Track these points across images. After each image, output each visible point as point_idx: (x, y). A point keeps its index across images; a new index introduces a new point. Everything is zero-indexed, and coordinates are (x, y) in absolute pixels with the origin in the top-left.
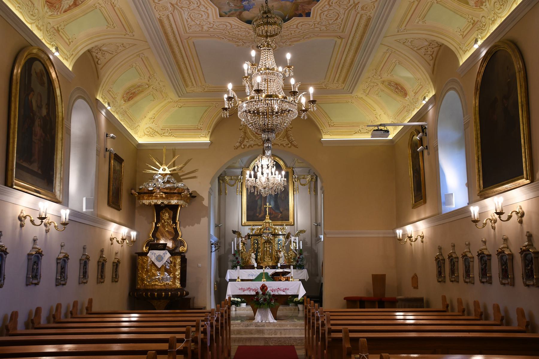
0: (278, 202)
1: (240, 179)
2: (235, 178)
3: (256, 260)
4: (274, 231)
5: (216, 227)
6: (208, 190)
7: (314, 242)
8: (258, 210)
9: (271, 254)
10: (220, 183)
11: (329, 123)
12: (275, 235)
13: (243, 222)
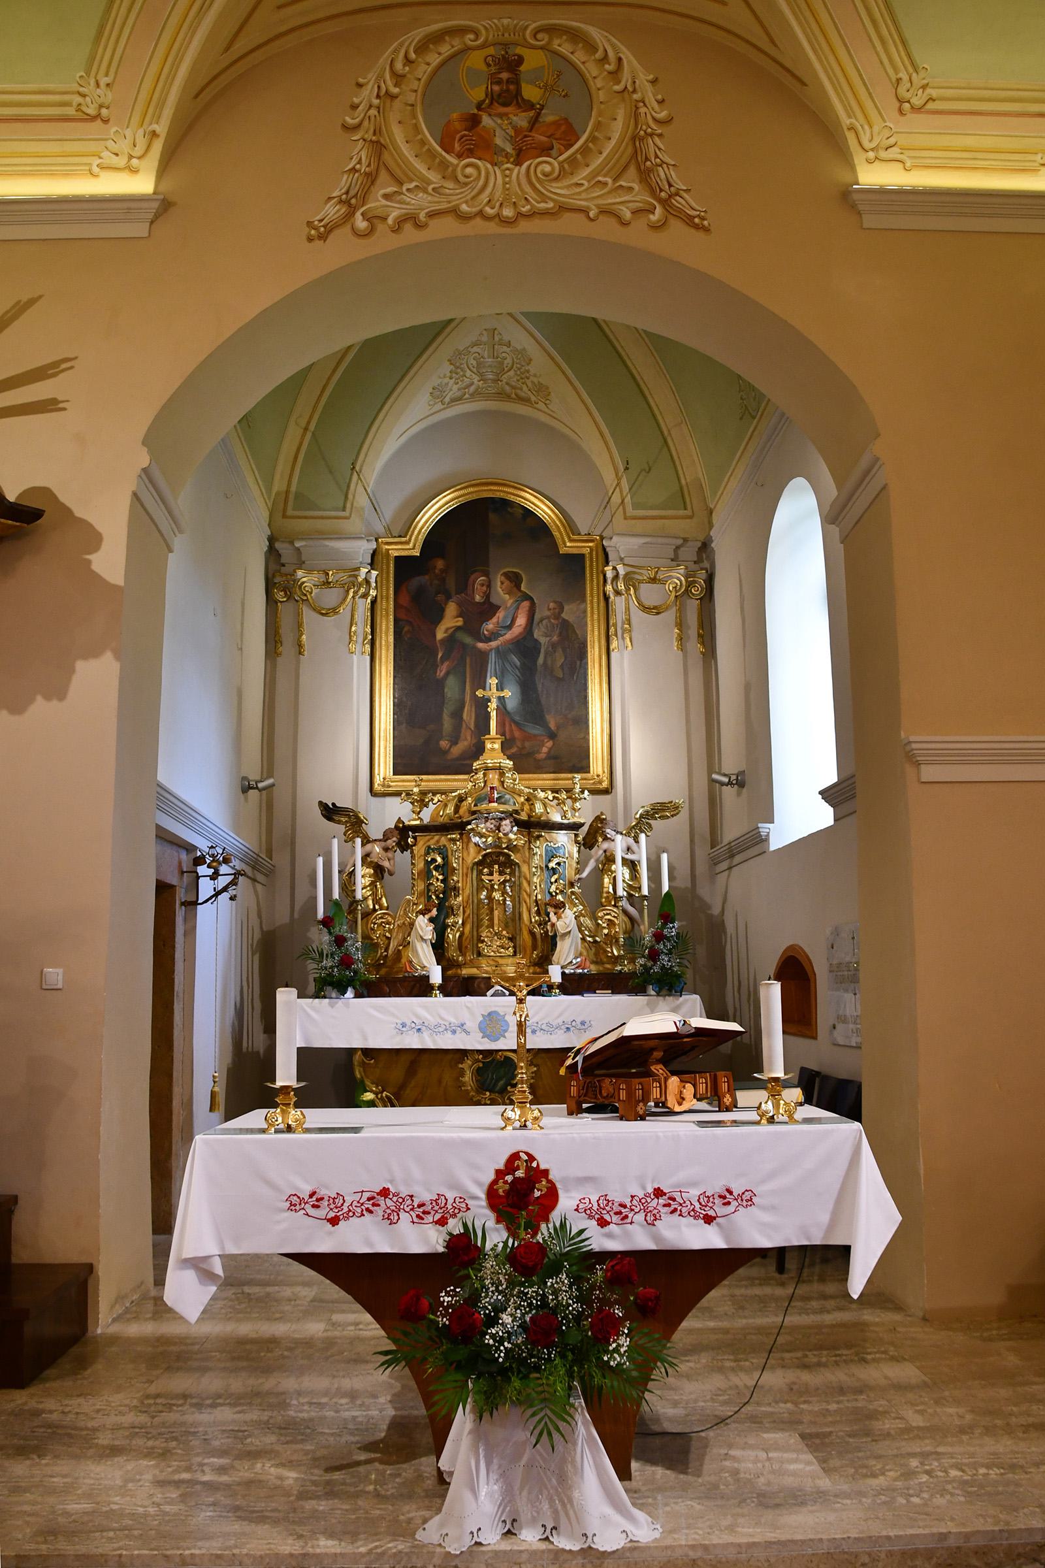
0: (540, 687)
1: (367, 582)
2: (344, 577)
3: (439, 947)
4: (526, 807)
6: (130, 484)
7: (702, 867)
8: (447, 723)
9: (513, 921)
10: (276, 602)
11: (902, 91)
12: (533, 826)
13: (378, 780)
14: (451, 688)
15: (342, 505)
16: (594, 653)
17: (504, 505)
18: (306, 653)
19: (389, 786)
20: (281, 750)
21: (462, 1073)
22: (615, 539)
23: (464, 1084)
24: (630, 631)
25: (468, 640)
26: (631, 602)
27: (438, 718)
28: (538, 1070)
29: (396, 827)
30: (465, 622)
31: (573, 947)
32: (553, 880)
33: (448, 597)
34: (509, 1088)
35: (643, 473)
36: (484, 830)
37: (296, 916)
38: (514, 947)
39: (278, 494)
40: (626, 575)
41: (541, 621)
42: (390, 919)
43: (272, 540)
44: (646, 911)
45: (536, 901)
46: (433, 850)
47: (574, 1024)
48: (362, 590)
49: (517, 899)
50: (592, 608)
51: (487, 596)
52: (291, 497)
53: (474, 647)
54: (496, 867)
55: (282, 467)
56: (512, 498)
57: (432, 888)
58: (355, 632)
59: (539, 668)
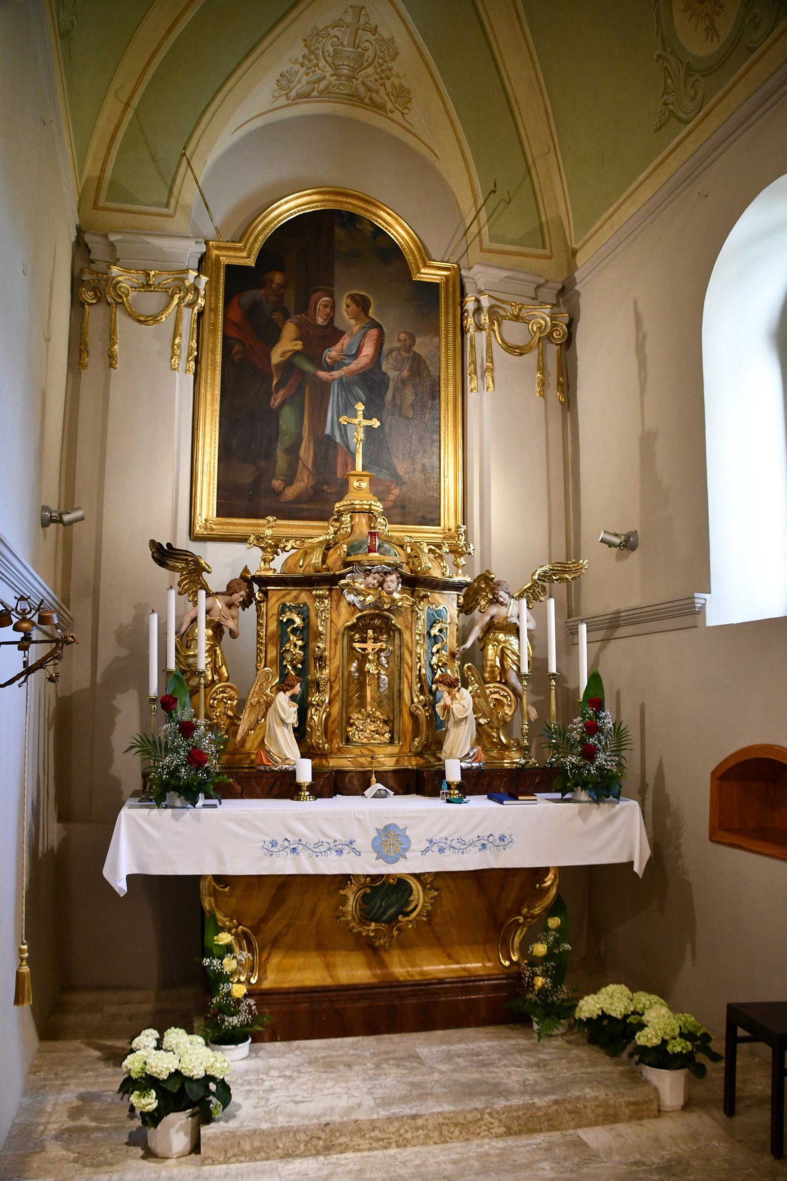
1: (197, 290)
2: (167, 279)
3: (301, 733)
5: (45, 523)
8: (281, 461)
10: (82, 304)
13: (200, 521)
14: (287, 420)
15: (165, 200)
16: (448, 393)
17: (350, 219)
18: (117, 366)
19: (212, 530)
20: (84, 482)
21: (344, 900)
22: (476, 268)
23: (344, 914)
24: (492, 370)
25: (308, 367)
27: (270, 456)
28: (440, 895)
29: (243, 577)
30: (304, 345)
31: (470, 736)
32: (434, 650)
33: (287, 317)
34: (400, 917)
35: (503, 204)
36: (362, 586)
37: (99, 680)
38: (392, 732)
39: (88, 180)
40: (492, 307)
41: (390, 352)
42: (233, 693)
43: (80, 231)
44: (553, 692)
45: (419, 676)
46: (290, 609)
47: (491, 839)
48: (190, 297)
49: (397, 674)
50: (447, 342)
51: (331, 320)
52: (105, 186)
53: (315, 376)
54: (370, 632)
55: (96, 147)
56: (361, 213)
58: (179, 346)
59: (386, 404)
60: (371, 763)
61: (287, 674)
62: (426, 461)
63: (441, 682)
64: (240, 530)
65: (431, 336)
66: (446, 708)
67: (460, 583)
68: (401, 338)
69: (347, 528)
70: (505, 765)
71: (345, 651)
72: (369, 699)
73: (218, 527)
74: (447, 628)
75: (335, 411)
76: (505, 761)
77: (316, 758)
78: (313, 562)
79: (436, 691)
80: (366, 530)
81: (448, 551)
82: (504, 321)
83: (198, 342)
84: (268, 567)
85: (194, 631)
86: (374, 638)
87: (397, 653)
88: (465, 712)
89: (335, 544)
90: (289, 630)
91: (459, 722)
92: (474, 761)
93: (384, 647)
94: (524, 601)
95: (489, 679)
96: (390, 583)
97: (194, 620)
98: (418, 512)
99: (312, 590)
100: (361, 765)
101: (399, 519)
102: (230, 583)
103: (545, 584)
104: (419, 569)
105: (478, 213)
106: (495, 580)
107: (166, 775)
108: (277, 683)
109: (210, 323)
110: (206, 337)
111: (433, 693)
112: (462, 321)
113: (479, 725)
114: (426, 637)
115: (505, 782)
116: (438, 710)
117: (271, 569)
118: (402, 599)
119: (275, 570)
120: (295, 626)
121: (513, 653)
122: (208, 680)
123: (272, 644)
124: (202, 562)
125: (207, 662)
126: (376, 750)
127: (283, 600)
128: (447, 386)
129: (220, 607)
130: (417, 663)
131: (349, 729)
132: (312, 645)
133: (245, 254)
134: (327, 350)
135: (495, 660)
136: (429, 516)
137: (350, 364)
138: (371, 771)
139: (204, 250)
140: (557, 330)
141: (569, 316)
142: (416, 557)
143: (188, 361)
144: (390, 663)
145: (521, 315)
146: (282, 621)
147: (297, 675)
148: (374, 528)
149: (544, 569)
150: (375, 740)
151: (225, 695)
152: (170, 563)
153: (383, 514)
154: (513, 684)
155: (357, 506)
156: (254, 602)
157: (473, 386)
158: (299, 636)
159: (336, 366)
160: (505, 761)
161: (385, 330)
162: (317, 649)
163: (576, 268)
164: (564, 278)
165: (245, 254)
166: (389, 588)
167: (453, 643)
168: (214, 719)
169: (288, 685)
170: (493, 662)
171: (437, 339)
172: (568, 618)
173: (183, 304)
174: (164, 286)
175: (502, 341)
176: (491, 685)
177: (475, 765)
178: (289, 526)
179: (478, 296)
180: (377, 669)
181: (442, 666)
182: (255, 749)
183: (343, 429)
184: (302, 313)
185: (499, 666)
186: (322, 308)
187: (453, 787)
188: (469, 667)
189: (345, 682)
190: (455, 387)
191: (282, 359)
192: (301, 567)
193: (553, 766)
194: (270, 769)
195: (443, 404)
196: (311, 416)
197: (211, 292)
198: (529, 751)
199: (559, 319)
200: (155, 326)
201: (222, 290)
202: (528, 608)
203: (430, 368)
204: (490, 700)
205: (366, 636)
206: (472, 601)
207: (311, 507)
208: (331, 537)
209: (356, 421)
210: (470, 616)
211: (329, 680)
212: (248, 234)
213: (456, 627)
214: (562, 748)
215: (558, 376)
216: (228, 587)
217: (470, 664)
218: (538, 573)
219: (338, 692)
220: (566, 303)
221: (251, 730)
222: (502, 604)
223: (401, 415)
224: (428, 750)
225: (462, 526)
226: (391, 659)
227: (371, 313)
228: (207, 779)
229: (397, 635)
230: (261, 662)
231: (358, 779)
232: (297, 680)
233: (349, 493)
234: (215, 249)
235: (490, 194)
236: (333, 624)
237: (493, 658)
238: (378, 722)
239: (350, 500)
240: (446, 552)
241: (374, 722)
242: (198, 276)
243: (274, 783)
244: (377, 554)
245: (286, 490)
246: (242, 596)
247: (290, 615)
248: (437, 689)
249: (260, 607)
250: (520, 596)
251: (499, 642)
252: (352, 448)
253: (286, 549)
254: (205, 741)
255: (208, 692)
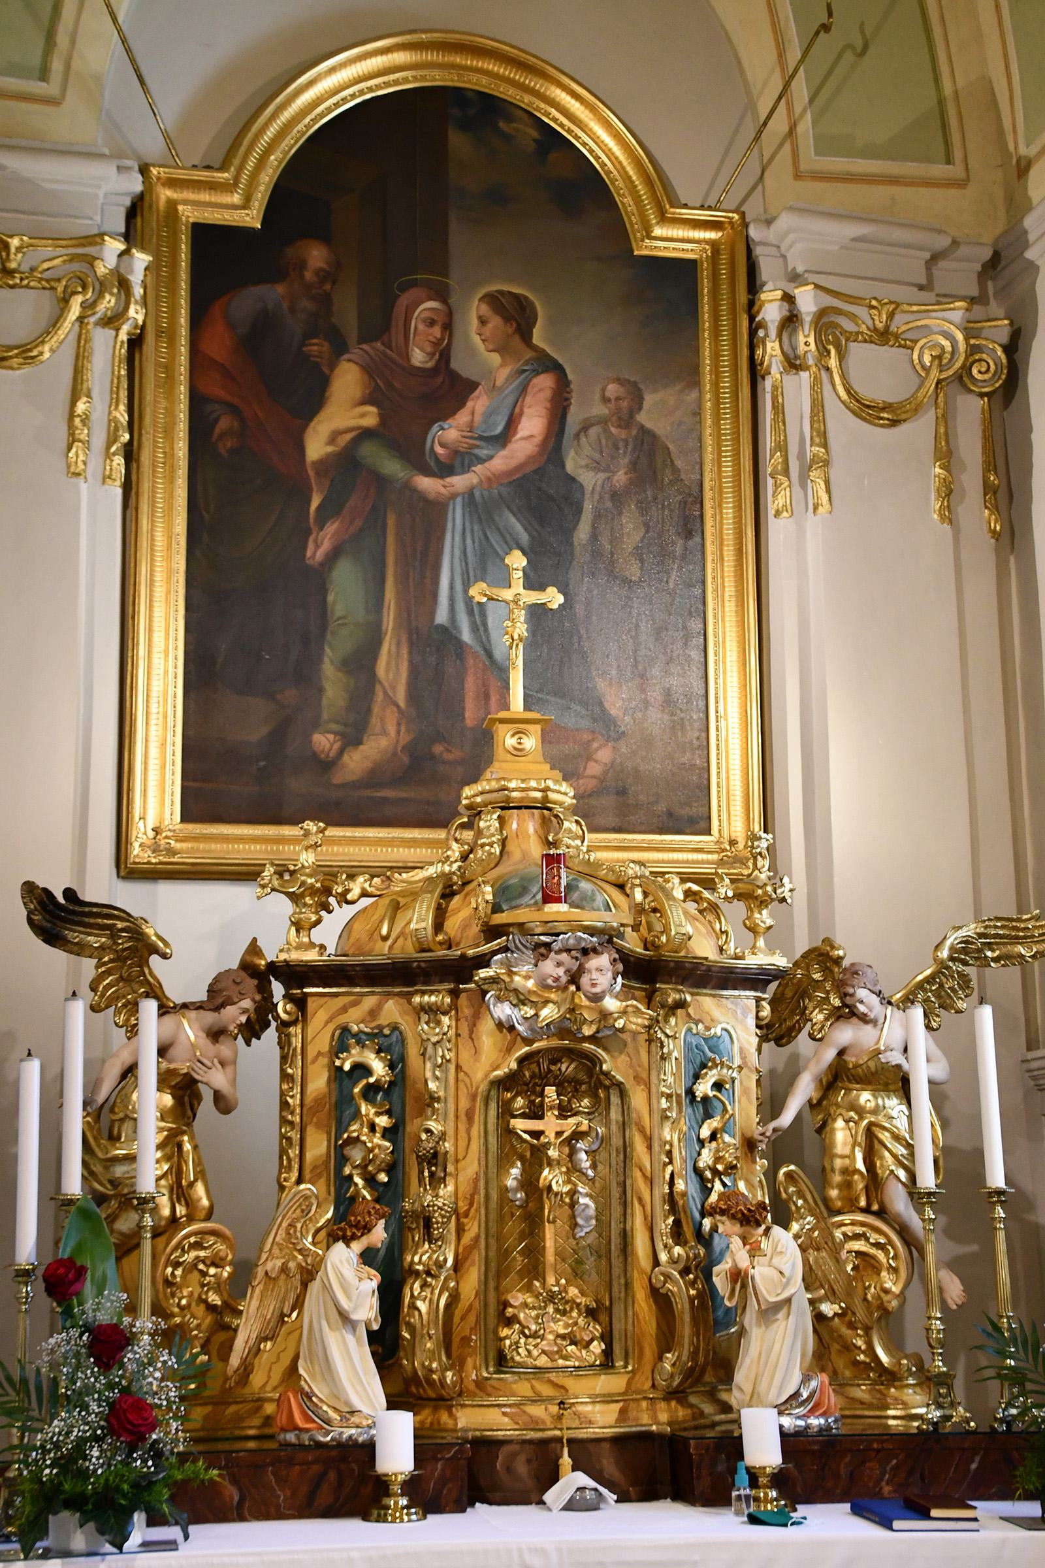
1: (124, 285)
13: (141, 833)
15: (36, 60)
19: (171, 852)
22: (785, 221)
24: (826, 463)
25: (392, 467)
26: (827, 387)
29: (247, 967)
30: (381, 416)
32: (705, 1132)
33: (340, 348)
35: (849, 56)
36: (530, 984)
40: (822, 313)
41: (585, 429)
42: (221, 1247)
44: (1001, 1236)
45: (671, 1198)
48: (109, 302)
49: (616, 1193)
50: (717, 401)
51: (444, 355)
53: (408, 487)
54: (551, 1091)
57: (357, 1155)
58: (86, 419)
59: (577, 550)
60: (560, 1417)
61: (353, 1199)
62: (674, 682)
63: (723, 1212)
64: (239, 851)
65: (678, 387)
66: (738, 1277)
67: (762, 970)
68: (607, 394)
69: (491, 845)
70: (891, 1422)
71: (493, 1140)
72: (550, 1256)
73: (184, 845)
74: (733, 1080)
75: (458, 570)
76: (891, 1412)
77: (422, 1407)
78: (413, 926)
79: (711, 1235)
80: (536, 850)
81: (730, 894)
82: (852, 345)
83: (130, 410)
84: (306, 940)
85: (128, 1097)
86: (561, 1107)
87: (616, 1141)
88: (785, 1286)
89: (465, 884)
90: (356, 1090)
91: (770, 1312)
92: (812, 1411)
93: (584, 1127)
94: (917, 1012)
95: (839, 1204)
96: (595, 975)
97: (130, 1071)
98: (657, 802)
99: (412, 994)
100: (535, 1424)
101: (612, 820)
102: (216, 980)
103: (967, 970)
104: (664, 939)
105: (787, 85)
106: (846, 963)
107: (52, 1466)
108: (329, 1221)
109: (158, 364)
110: (149, 397)
111: (705, 1240)
112: (752, 348)
113: (819, 1318)
114: (685, 1101)
115: (894, 1469)
116: (719, 1281)
117: (312, 945)
118: (624, 1013)
119: (323, 947)
120: (372, 1080)
121: (897, 1138)
122: (161, 1218)
123: (318, 1126)
124: (150, 931)
125: (159, 1173)
126: (569, 1383)
127: (342, 1019)
128: (720, 506)
129: (192, 1038)
130: (665, 1165)
131: (505, 1332)
132: (412, 1126)
133: (236, 198)
134: (435, 427)
135: (852, 1157)
136: (683, 812)
137: (491, 457)
138: (559, 1440)
139: (138, 187)
140: (980, 360)
141: (1011, 324)
142: (655, 910)
143: (108, 455)
144: (600, 1167)
145: (893, 328)
146: (340, 1068)
147: (377, 1200)
148: (555, 844)
149: (962, 933)
150: (566, 1358)
151: (202, 1254)
152: (70, 935)
153: (575, 810)
154: (899, 1215)
155: (515, 794)
156: (274, 1024)
157: (780, 501)
158: (381, 1105)
159: (457, 463)
160: (891, 1412)
161: (570, 376)
162: (424, 1136)
163: (1027, 207)
164: (998, 231)
165: (236, 198)
166: (594, 985)
167: (748, 1115)
168: (173, 1315)
169: (356, 1225)
170: (847, 1161)
171: (694, 395)
172: (1029, 1049)
173: (92, 320)
174: (45, 275)
175: (848, 392)
176: (847, 1218)
177: (816, 1422)
178: (353, 841)
179: (789, 288)
180: (569, 1181)
181: (725, 1173)
182: (275, 1389)
183: (477, 613)
184: (377, 340)
185: (863, 1170)
186: (421, 327)
187: (763, 1480)
188: (789, 1175)
189: (493, 1216)
190: (738, 508)
191: (330, 449)
192: (385, 939)
193: (1014, 1429)
194: (311, 1439)
195: (710, 548)
196: (403, 581)
197: (157, 290)
198: (950, 1388)
199: (985, 333)
200: (27, 370)
201: (184, 286)
202: (928, 1027)
203: (679, 463)
204: (844, 1255)
205: (542, 1103)
206: (793, 1013)
207: (404, 795)
208: (455, 866)
209: (508, 594)
210: (788, 1050)
211: (456, 1211)
212: (242, 149)
213: (755, 1077)
214: (1031, 1381)
215: (986, 472)
216: (212, 991)
217: (792, 1167)
218: (948, 943)
219: (476, 1239)
220: (1000, 293)
221: (266, 1339)
222: (864, 1019)
223: (612, 574)
224: (698, 1381)
225: (764, 835)
226: (602, 1156)
227: (538, 337)
228: (156, 1473)
229: (615, 1099)
230: (289, 1168)
231: (529, 1461)
232: (377, 1212)
233: (496, 764)
234: (164, 185)
235: (817, 33)
236: (461, 1075)
237: (847, 1151)
238: (575, 1314)
239: (498, 780)
240: (726, 898)
241: (564, 1313)
242: (125, 253)
243: (322, 1476)
244: (563, 907)
245: (346, 758)
246: (245, 1011)
247: (360, 1054)
248: (714, 1229)
249: (288, 1035)
250: (908, 1001)
251: (861, 1112)
252: (498, 654)
253: (349, 897)
254: (151, 1375)
255: (160, 1247)
